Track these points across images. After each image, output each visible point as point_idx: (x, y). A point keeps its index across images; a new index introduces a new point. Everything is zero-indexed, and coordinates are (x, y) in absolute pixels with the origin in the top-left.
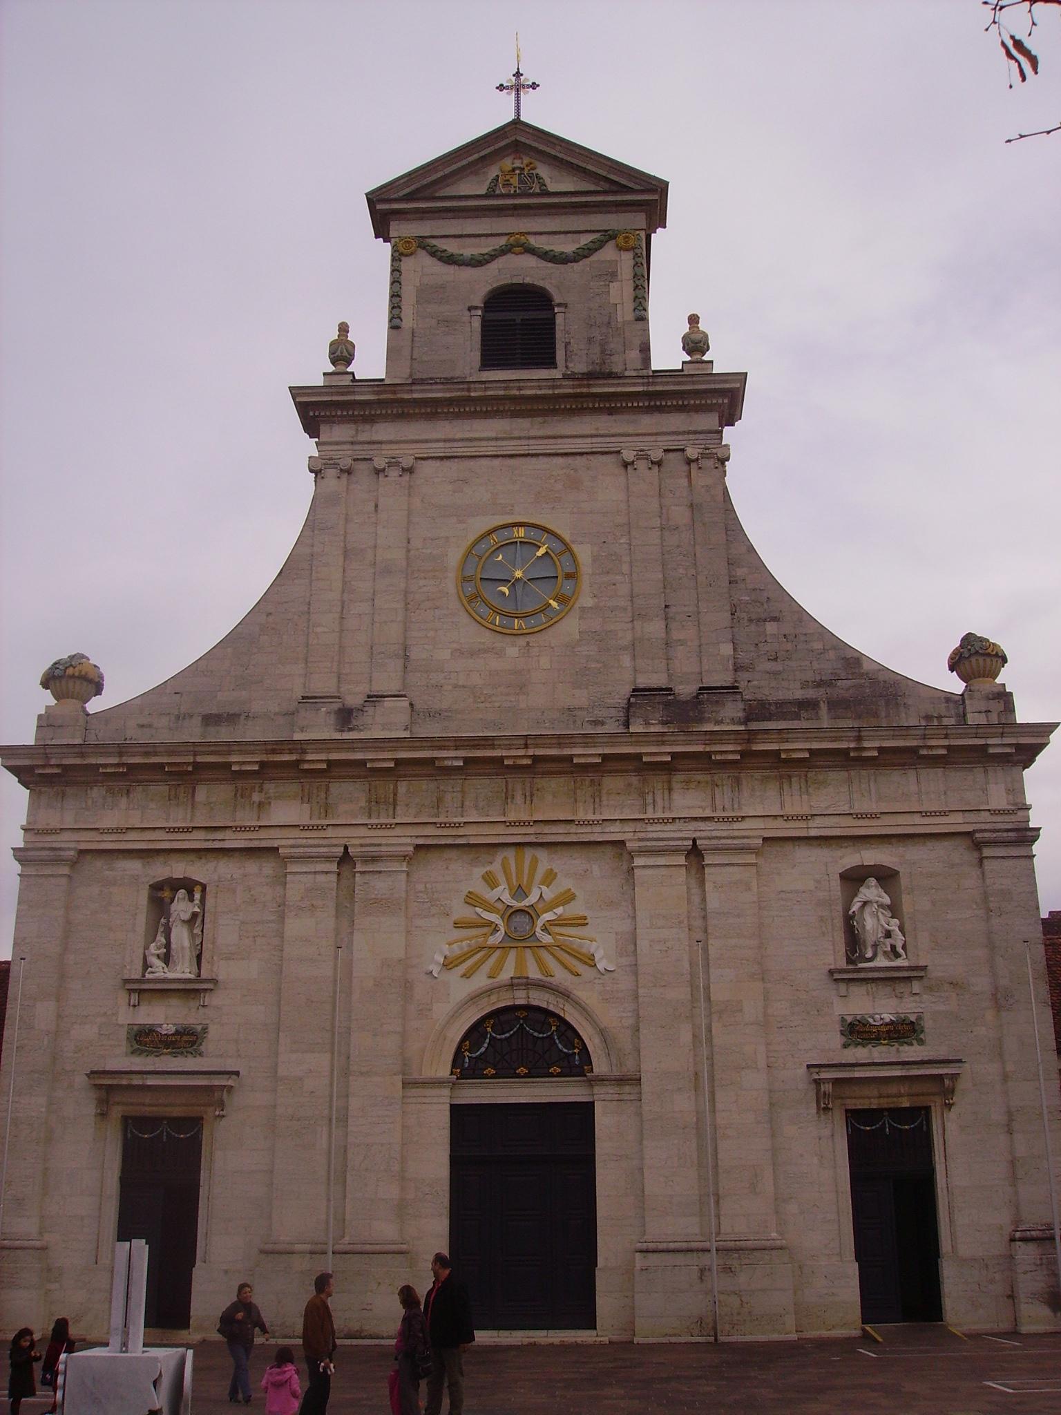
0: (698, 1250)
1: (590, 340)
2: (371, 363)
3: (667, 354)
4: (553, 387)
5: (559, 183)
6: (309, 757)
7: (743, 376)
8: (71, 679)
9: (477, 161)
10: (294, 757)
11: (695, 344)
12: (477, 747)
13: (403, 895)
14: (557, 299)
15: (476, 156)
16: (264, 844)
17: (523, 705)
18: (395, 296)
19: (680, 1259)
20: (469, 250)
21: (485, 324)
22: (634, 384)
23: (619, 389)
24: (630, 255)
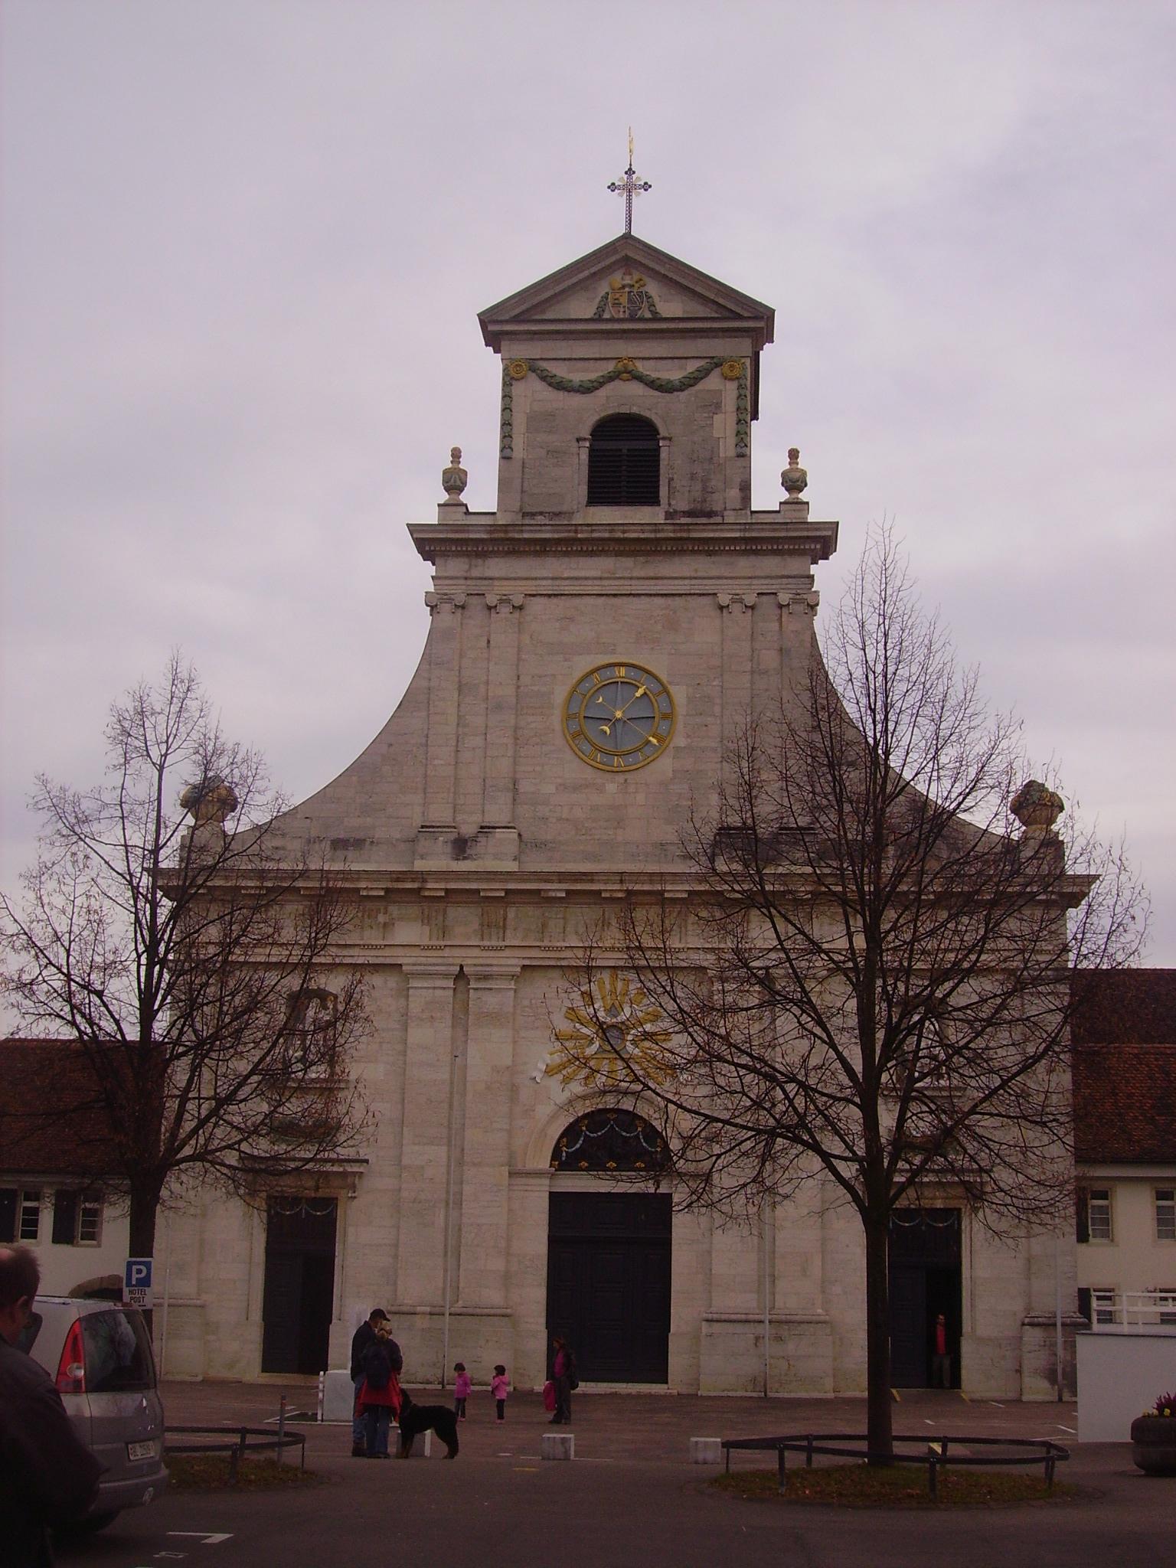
0: (755, 1321)
1: (693, 477)
2: (483, 496)
3: (767, 495)
4: (655, 531)
5: (671, 306)
6: (429, 886)
7: (837, 523)
8: (210, 798)
9: (587, 278)
10: (416, 885)
11: (794, 482)
12: (576, 881)
13: (511, 1010)
14: (663, 432)
15: (586, 273)
16: (388, 961)
17: (620, 839)
18: (506, 424)
19: (739, 1328)
20: (577, 377)
21: (591, 450)
22: (732, 530)
23: (717, 535)
24: (735, 384)
